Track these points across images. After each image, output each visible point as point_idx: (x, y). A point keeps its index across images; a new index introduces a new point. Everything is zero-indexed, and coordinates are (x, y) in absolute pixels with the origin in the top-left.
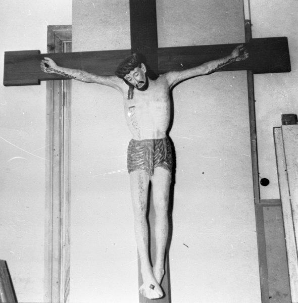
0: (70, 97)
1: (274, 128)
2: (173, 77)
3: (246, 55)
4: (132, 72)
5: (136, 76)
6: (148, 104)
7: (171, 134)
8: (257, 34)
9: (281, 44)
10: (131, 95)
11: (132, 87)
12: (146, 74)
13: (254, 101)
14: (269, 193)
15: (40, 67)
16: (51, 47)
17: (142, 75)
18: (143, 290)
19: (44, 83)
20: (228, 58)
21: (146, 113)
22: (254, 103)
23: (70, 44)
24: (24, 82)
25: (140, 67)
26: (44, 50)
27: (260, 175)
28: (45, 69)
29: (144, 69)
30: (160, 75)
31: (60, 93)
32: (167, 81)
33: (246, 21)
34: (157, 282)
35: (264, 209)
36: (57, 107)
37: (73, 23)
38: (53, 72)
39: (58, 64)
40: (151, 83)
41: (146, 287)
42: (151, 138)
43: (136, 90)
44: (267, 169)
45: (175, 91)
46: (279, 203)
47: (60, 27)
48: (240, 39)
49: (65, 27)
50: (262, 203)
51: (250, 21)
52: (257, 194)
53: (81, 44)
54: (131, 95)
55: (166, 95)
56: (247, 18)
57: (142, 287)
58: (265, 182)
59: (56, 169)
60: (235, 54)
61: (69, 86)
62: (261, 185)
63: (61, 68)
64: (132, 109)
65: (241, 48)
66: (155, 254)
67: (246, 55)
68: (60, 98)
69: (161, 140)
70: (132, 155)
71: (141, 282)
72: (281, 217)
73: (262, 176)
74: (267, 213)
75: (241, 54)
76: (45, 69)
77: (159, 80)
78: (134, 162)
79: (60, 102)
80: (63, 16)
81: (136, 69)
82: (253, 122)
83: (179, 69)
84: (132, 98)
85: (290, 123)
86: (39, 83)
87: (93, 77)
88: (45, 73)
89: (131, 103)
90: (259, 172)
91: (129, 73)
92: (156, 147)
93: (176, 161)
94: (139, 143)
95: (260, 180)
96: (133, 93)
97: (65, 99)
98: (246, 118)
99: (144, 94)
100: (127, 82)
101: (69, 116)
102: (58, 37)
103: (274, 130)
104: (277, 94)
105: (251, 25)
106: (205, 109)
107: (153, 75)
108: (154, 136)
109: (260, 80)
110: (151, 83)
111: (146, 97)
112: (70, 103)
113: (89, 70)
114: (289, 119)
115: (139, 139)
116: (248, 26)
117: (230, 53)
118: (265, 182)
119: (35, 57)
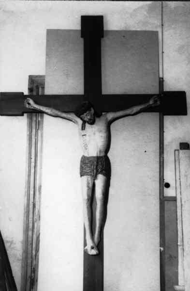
0: (42, 124)
1: (175, 150)
2: (110, 116)
3: (158, 103)
4: (85, 114)
5: (87, 117)
6: (94, 134)
7: (109, 155)
8: (167, 88)
9: (180, 95)
10: (83, 128)
11: (84, 122)
12: (94, 114)
13: (163, 132)
14: (169, 192)
15: (24, 105)
16: (31, 90)
17: (91, 115)
18: (87, 249)
19: (25, 115)
20: (148, 104)
21: (92, 140)
22: (163, 134)
23: (43, 88)
24: (11, 113)
25: (90, 110)
26: (26, 93)
27: (165, 181)
28: (27, 106)
29: (93, 111)
30: (103, 113)
31: (36, 121)
32: (107, 119)
33: (160, 78)
34: (98, 147)
35: (166, 202)
36: (34, 131)
37: (46, 72)
38: (32, 108)
39: (36, 103)
40: (97, 120)
41: (89, 247)
42: (95, 155)
43: (87, 125)
44: (169, 177)
45: (113, 126)
46: (174, 199)
47: (37, 76)
48: (154, 90)
49: (41, 76)
50: (165, 199)
51: (163, 78)
52: (161, 192)
53: (52, 89)
54: (83, 128)
55: (105, 128)
56: (161, 76)
57: (86, 248)
58: (168, 185)
59: (33, 171)
60: (151, 102)
61: (42, 117)
62: (164, 188)
63: (38, 106)
64: (84, 136)
65: (155, 98)
66: (96, 209)
67: (158, 103)
68: (36, 125)
69: (102, 157)
70: (83, 166)
71: (85, 245)
72: (175, 208)
73: (166, 181)
74: (168, 205)
75: (155, 101)
76: (27, 106)
77: (102, 118)
78: (84, 170)
79: (35, 126)
80: (39, 70)
81: (88, 112)
82: (162, 160)
83: (114, 111)
84: (84, 129)
85: (184, 149)
86: (22, 115)
87: (59, 113)
88: (27, 108)
89: (83, 133)
90: (164, 178)
91: (83, 114)
92: (99, 161)
93: (110, 179)
94: (88, 158)
95: (164, 183)
96: (85, 126)
97: (39, 125)
98: (155, 181)
99: (92, 127)
100: (81, 119)
101: (42, 136)
102: (36, 83)
103: (175, 152)
104: (177, 129)
105: (163, 81)
106: (133, 147)
107: (97, 115)
108: (97, 154)
109: (168, 120)
110: (97, 120)
111: (94, 129)
112: (42, 127)
113: (55, 107)
114: (183, 146)
115: (88, 156)
116: (161, 82)
117: (148, 101)
118: (168, 185)
119: (19, 96)
